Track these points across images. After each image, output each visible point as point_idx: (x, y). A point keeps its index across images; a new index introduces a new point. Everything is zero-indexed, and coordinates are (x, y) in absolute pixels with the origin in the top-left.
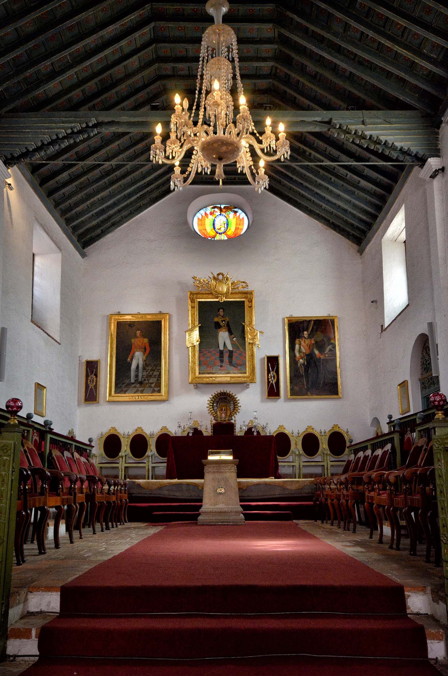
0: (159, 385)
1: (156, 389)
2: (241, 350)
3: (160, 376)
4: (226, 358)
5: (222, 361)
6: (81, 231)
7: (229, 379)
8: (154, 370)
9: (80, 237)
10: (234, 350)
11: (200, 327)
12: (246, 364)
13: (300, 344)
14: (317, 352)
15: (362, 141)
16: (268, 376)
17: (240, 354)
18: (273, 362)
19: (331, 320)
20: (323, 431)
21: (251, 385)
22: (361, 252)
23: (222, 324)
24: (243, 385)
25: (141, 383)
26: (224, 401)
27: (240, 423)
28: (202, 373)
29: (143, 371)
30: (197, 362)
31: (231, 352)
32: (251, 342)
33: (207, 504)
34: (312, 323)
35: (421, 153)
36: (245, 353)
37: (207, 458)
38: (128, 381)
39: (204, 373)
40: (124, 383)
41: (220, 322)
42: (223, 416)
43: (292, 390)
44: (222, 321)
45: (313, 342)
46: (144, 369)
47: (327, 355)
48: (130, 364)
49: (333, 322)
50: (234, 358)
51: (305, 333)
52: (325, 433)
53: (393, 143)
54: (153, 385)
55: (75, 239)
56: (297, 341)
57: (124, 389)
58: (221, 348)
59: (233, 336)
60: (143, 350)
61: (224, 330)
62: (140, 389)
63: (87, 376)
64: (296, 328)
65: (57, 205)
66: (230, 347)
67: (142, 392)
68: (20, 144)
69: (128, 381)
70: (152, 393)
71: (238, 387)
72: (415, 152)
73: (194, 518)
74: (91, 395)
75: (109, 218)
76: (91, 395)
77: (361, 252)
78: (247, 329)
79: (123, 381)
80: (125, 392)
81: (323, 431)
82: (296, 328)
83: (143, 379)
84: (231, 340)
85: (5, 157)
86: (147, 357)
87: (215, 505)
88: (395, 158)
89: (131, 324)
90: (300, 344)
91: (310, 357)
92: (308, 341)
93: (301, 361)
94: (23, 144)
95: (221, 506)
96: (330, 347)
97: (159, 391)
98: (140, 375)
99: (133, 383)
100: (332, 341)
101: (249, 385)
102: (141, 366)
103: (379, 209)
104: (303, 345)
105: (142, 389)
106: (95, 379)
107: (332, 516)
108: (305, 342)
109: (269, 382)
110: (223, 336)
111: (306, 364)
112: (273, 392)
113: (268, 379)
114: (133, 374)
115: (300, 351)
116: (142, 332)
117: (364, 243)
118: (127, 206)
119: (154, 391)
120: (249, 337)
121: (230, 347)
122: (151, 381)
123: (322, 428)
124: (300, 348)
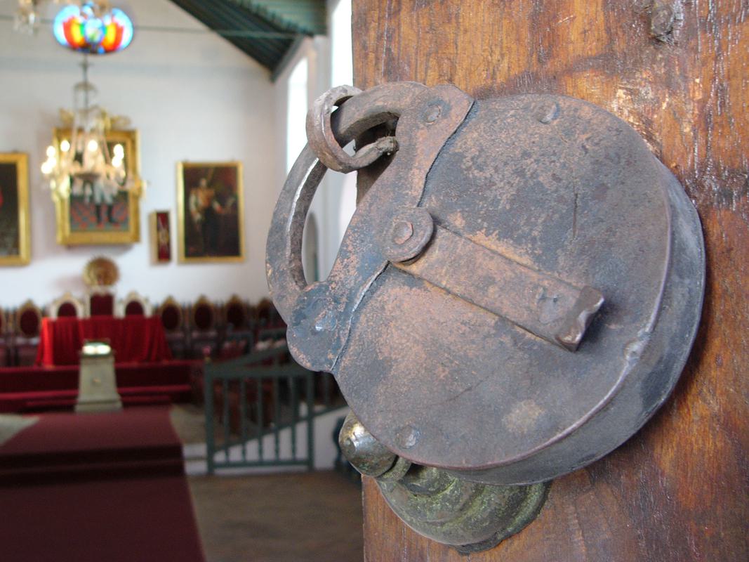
18: (163, 218)
24: (124, 247)
27: (122, 292)
42: (99, 289)
64: (193, 176)
82: (193, 176)
91: (208, 211)
95: (99, 396)
112: (163, 255)
115: (196, 204)
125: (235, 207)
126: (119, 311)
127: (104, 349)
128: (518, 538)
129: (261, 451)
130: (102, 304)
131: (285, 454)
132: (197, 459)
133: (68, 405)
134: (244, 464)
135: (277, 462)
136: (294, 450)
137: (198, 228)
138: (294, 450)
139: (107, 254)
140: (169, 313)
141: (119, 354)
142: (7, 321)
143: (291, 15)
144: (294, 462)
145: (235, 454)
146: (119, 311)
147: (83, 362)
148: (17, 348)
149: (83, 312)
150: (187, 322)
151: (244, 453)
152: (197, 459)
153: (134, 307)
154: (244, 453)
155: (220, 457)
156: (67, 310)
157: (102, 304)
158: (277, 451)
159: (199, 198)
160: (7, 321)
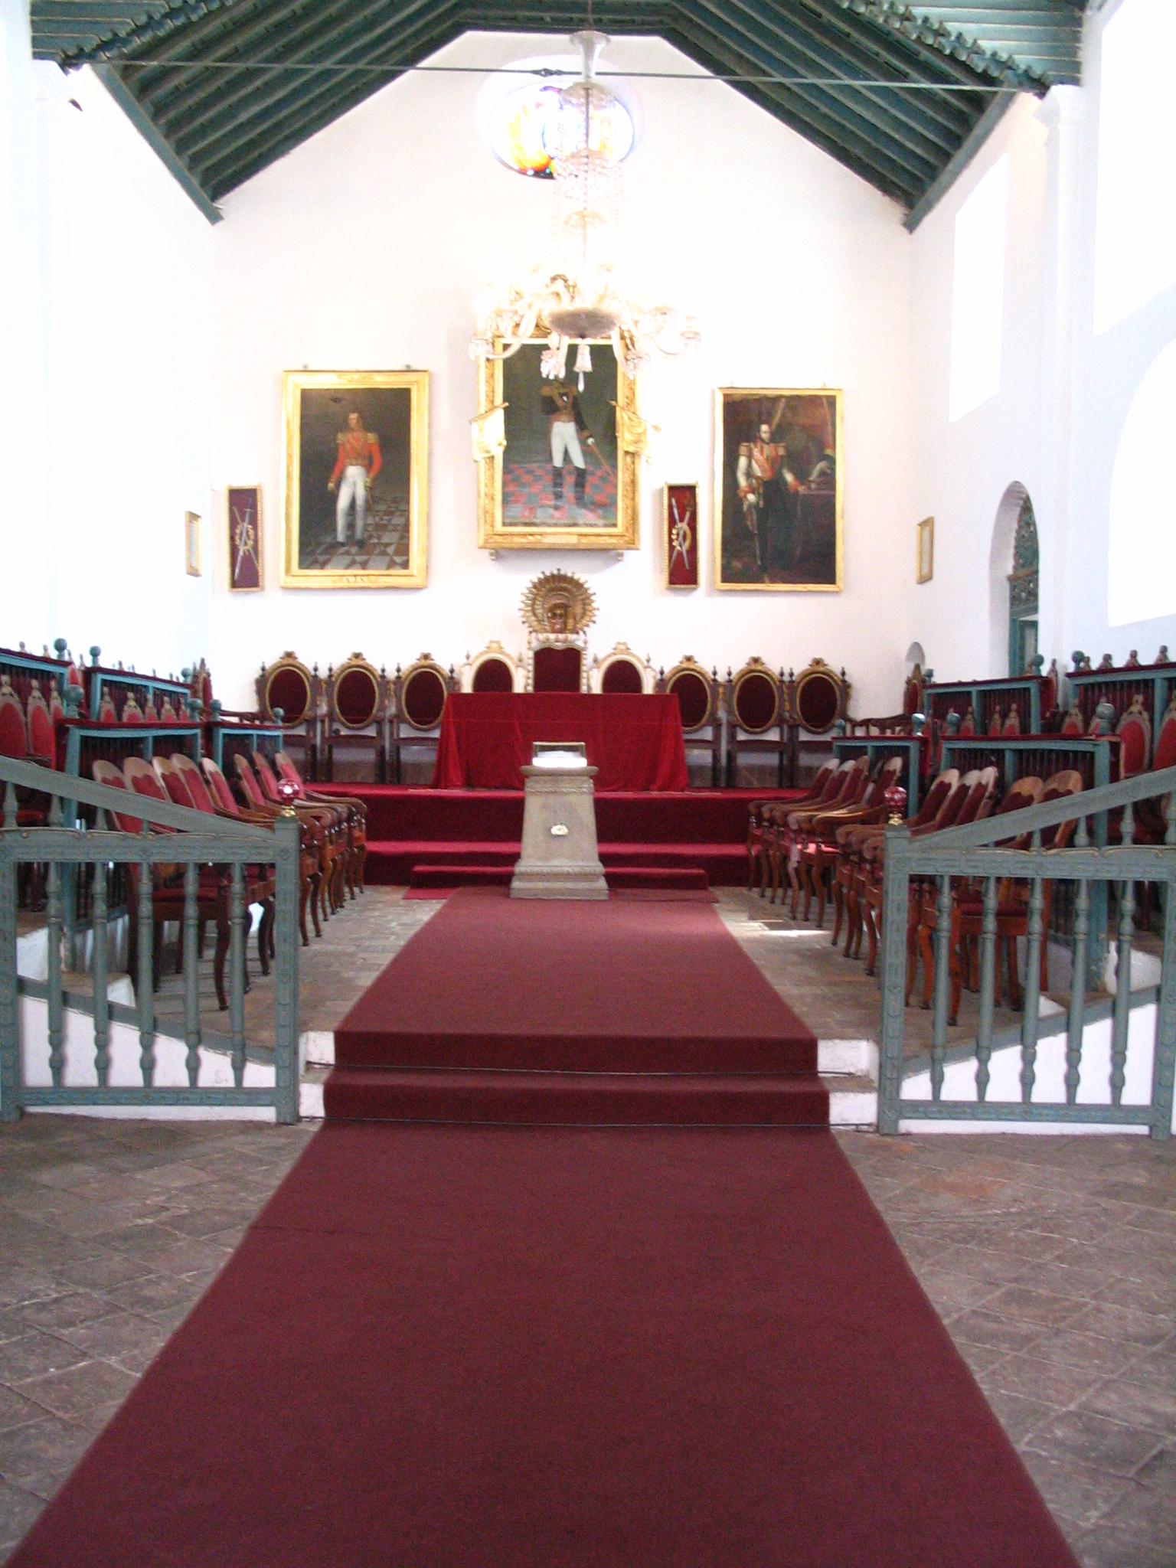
0: (404, 549)
1: (398, 559)
2: (607, 468)
3: (406, 528)
4: (568, 491)
5: (558, 496)
6: (208, 163)
7: (574, 540)
8: (391, 513)
9: (206, 178)
10: (591, 468)
11: (506, 409)
12: (614, 504)
13: (750, 457)
14: (789, 477)
15: (906, 23)
16: (670, 533)
17: (603, 479)
18: (682, 498)
19: (827, 397)
20: (787, 671)
21: (629, 555)
22: (911, 224)
23: (560, 403)
24: (608, 553)
25: (361, 544)
26: (560, 600)
27: (597, 647)
28: (511, 525)
29: (366, 515)
30: (499, 497)
31: (581, 474)
32: (631, 449)
33: (529, 857)
34: (782, 404)
35: (1037, 71)
36: (616, 475)
37: (529, 763)
38: (328, 539)
39: (515, 525)
40: (320, 544)
41: (556, 398)
42: (556, 640)
43: (725, 568)
44: (561, 395)
45: (781, 452)
46: (368, 508)
47: (813, 486)
48: (334, 497)
49: (831, 401)
50: (592, 486)
51: (764, 428)
52: (791, 675)
53: (975, 41)
54: (390, 550)
55: (195, 181)
56: (743, 449)
57: (321, 558)
58: (558, 461)
59: (586, 433)
60: (366, 462)
61: (565, 418)
62: (359, 558)
63: (233, 524)
64: (743, 417)
65: (158, 110)
66: (579, 461)
67: (364, 565)
68: (97, 23)
69: (328, 539)
70: (388, 568)
71: (596, 562)
72: (1023, 67)
73: (505, 880)
74: (245, 574)
75: (279, 126)
76: (245, 574)
77: (911, 225)
78: (621, 416)
79: (319, 538)
80: (323, 565)
81: (787, 671)
82: (743, 417)
83: (366, 535)
84: (583, 442)
85: (64, 52)
86: (374, 480)
87: (547, 859)
88: (979, 70)
89: (336, 397)
90: (750, 457)
91: (772, 488)
92: (768, 450)
93: (751, 497)
94: (105, 23)
95: (562, 864)
96: (821, 465)
97: (405, 565)
98: (359, 524)
99: (343, 545)
100: (828, 452)
101: (622, 555)
102: (360, 502)
103: (957, 141)
104: (755, 461)
105: (364, 558)
106: (251, 532)
107: (765, 880)
108: (762, 451)
109: (671, 548)
110: (564, 435)
111: (761, 503)
112: (682, 573)
113: (671, 541)
114: (341, 521)
115: (749, 474)
116: (362, 417)
117: (921, 203)
118: (321, 96)
119: (392, 565)
120: (625, 441)
121: (579, 461)
122: (385, 540)
123: (787, 660)
124: (750, 465)
125: (828, 480)
126: (593, 681)
127: (575, 762)
128: (268, 666)
129: (1027, 1080)
130: (558, 666)
131: (1094, 1090)
132: (853, 1082)
133: (496, 875)
134: (979, 1108)
135: (1070, 1109)
136: (1117, 1083)
137: (751, 523)
138: (1117, 1083)
139: (571, 568)
140: (689, 690)
141: (605, 774)
142: (383, 695)
143: (994, 37)
144: (1116, 1111)
145: (958, 1080)
146: (593, 681)
147: (530, 785)
148: (399, 744)
149: (522, 681)
150: (788, 707)
151: (982, 1080)
152: (853, 1082)
153: (622, 675)
154: (982, 1080)
155: (916, 1087)
156: (493, 674)
157: (558, 666)
158: (1072, 1081)
159: (755, 461)
160: (383, 695)
